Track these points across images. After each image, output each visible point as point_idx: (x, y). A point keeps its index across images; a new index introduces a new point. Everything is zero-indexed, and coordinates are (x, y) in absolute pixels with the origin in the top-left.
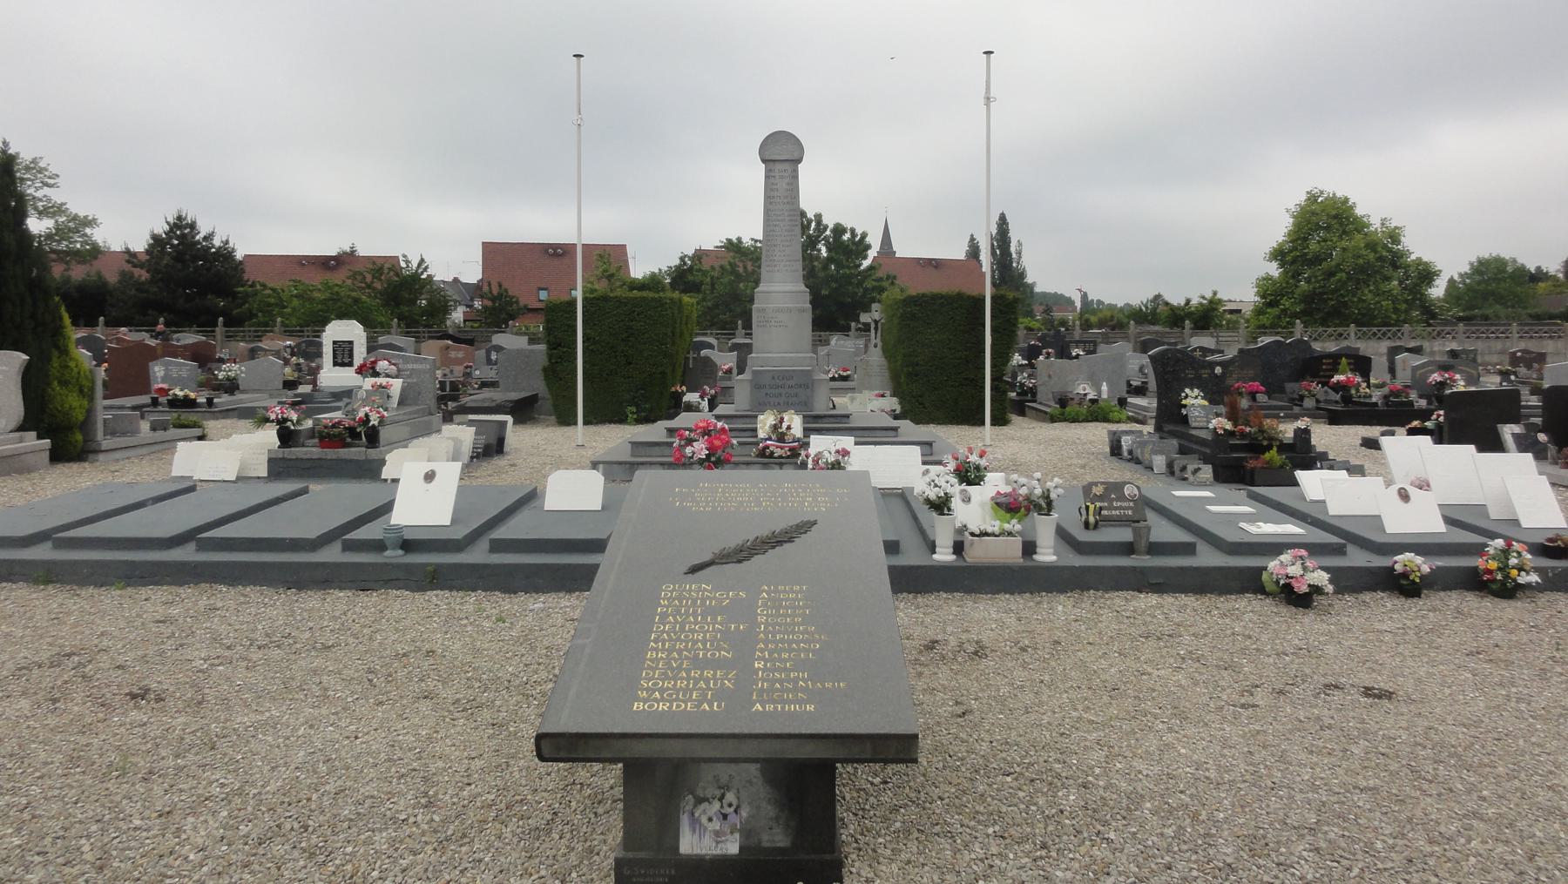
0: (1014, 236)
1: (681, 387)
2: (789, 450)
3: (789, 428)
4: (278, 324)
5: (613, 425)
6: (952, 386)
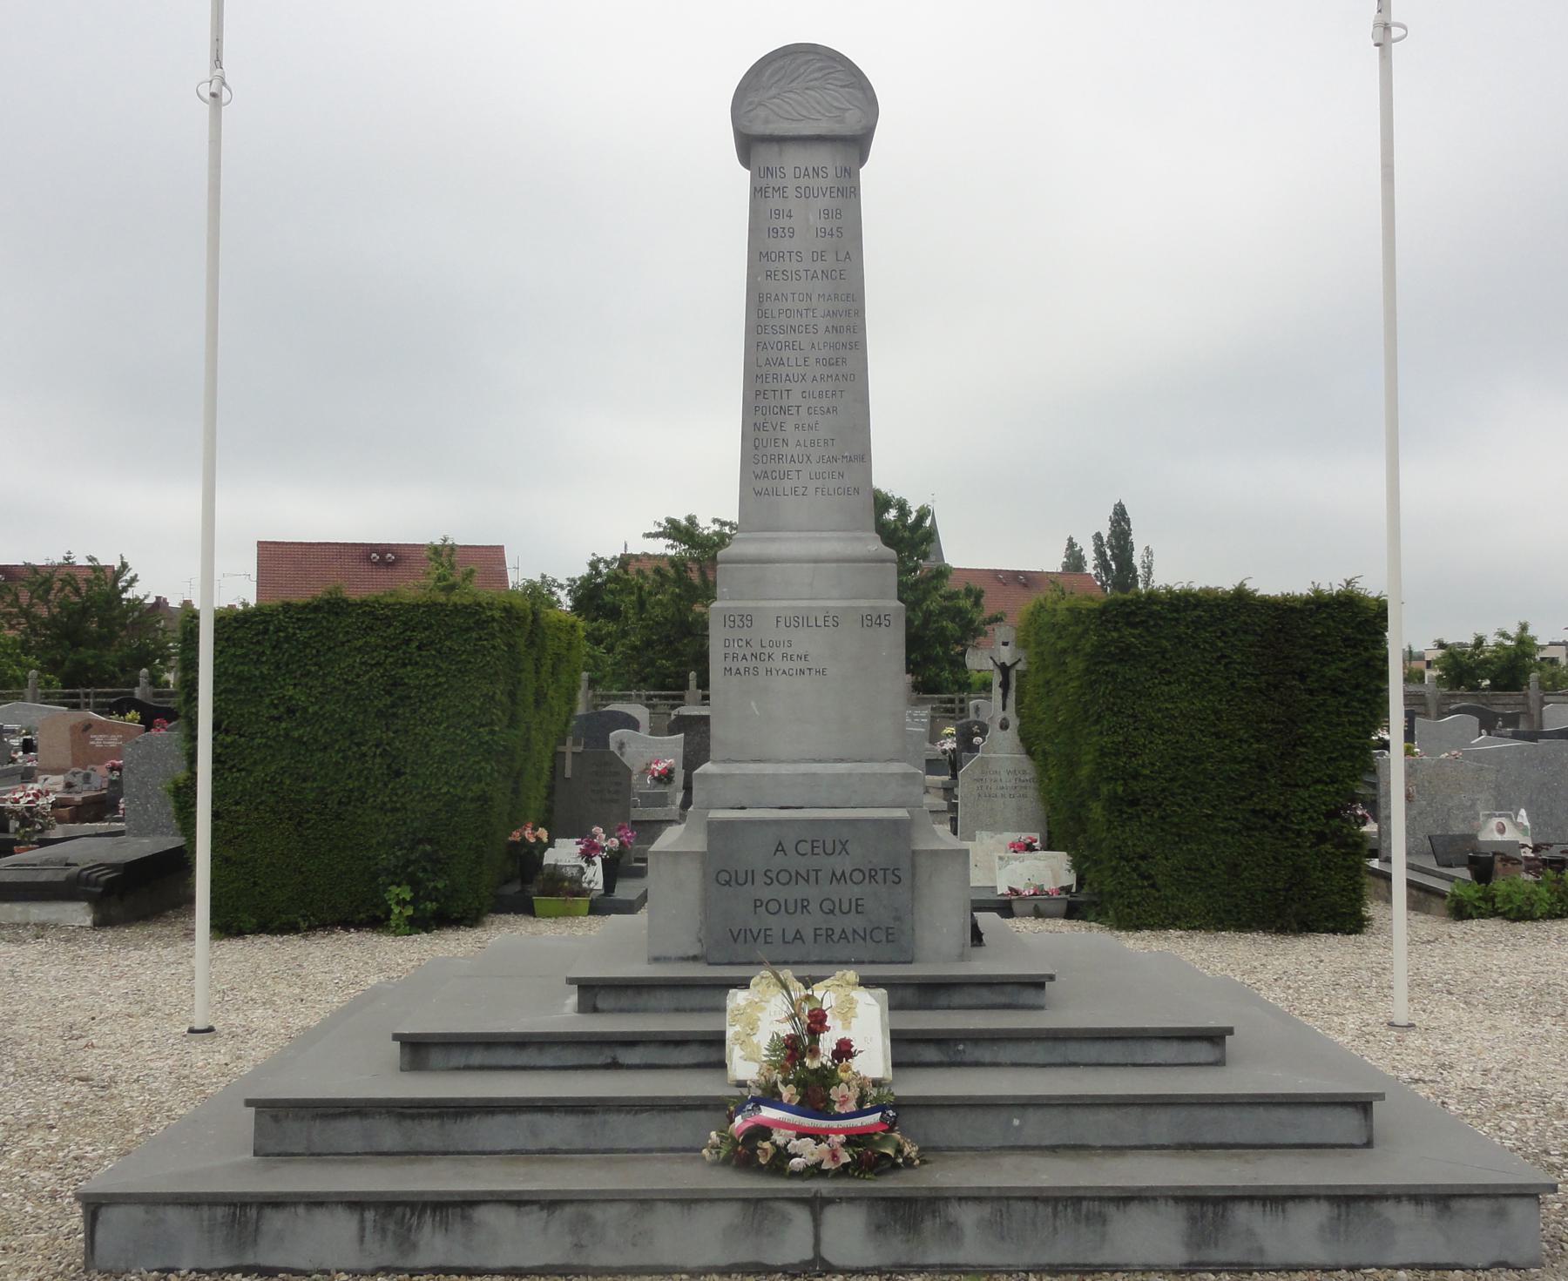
0: (1139, 541)
1: (535, 829)
2: (845, 1145)
3: (844, 1051)
4: (142, 681)
5: (354, 936)
6: (1225, 831)
